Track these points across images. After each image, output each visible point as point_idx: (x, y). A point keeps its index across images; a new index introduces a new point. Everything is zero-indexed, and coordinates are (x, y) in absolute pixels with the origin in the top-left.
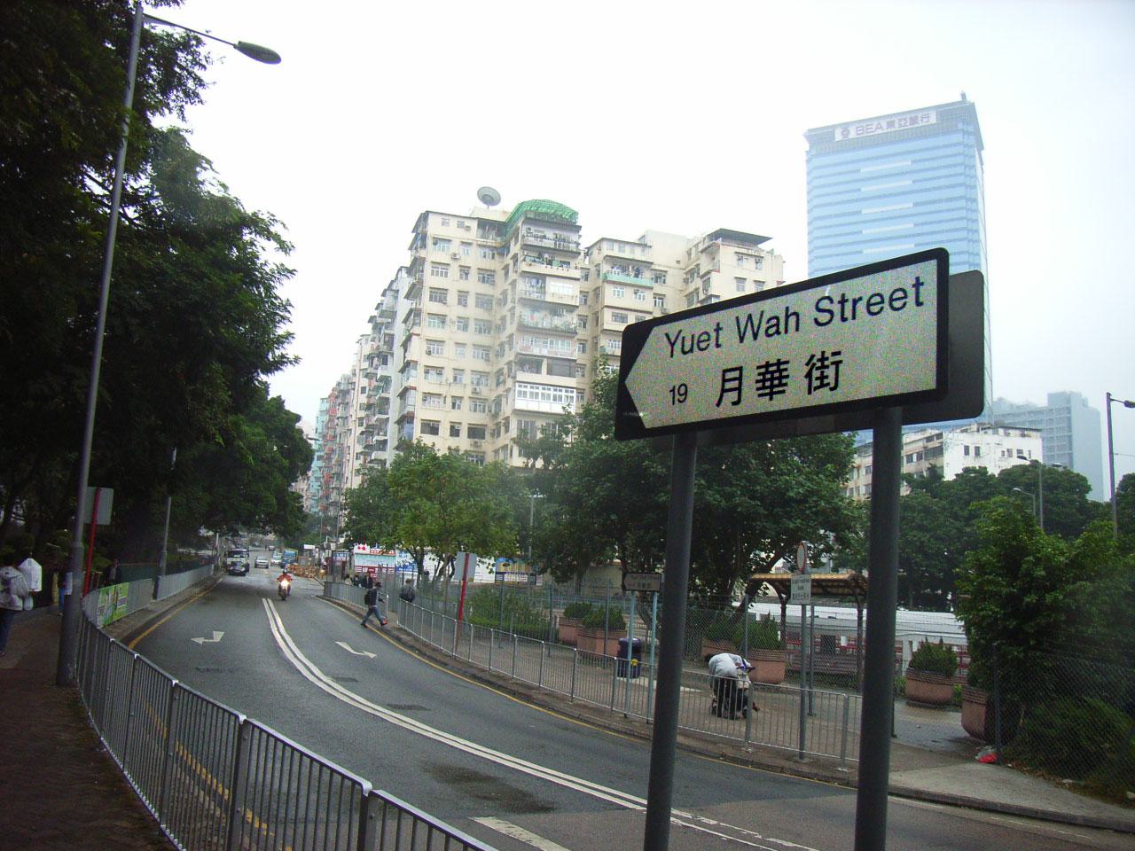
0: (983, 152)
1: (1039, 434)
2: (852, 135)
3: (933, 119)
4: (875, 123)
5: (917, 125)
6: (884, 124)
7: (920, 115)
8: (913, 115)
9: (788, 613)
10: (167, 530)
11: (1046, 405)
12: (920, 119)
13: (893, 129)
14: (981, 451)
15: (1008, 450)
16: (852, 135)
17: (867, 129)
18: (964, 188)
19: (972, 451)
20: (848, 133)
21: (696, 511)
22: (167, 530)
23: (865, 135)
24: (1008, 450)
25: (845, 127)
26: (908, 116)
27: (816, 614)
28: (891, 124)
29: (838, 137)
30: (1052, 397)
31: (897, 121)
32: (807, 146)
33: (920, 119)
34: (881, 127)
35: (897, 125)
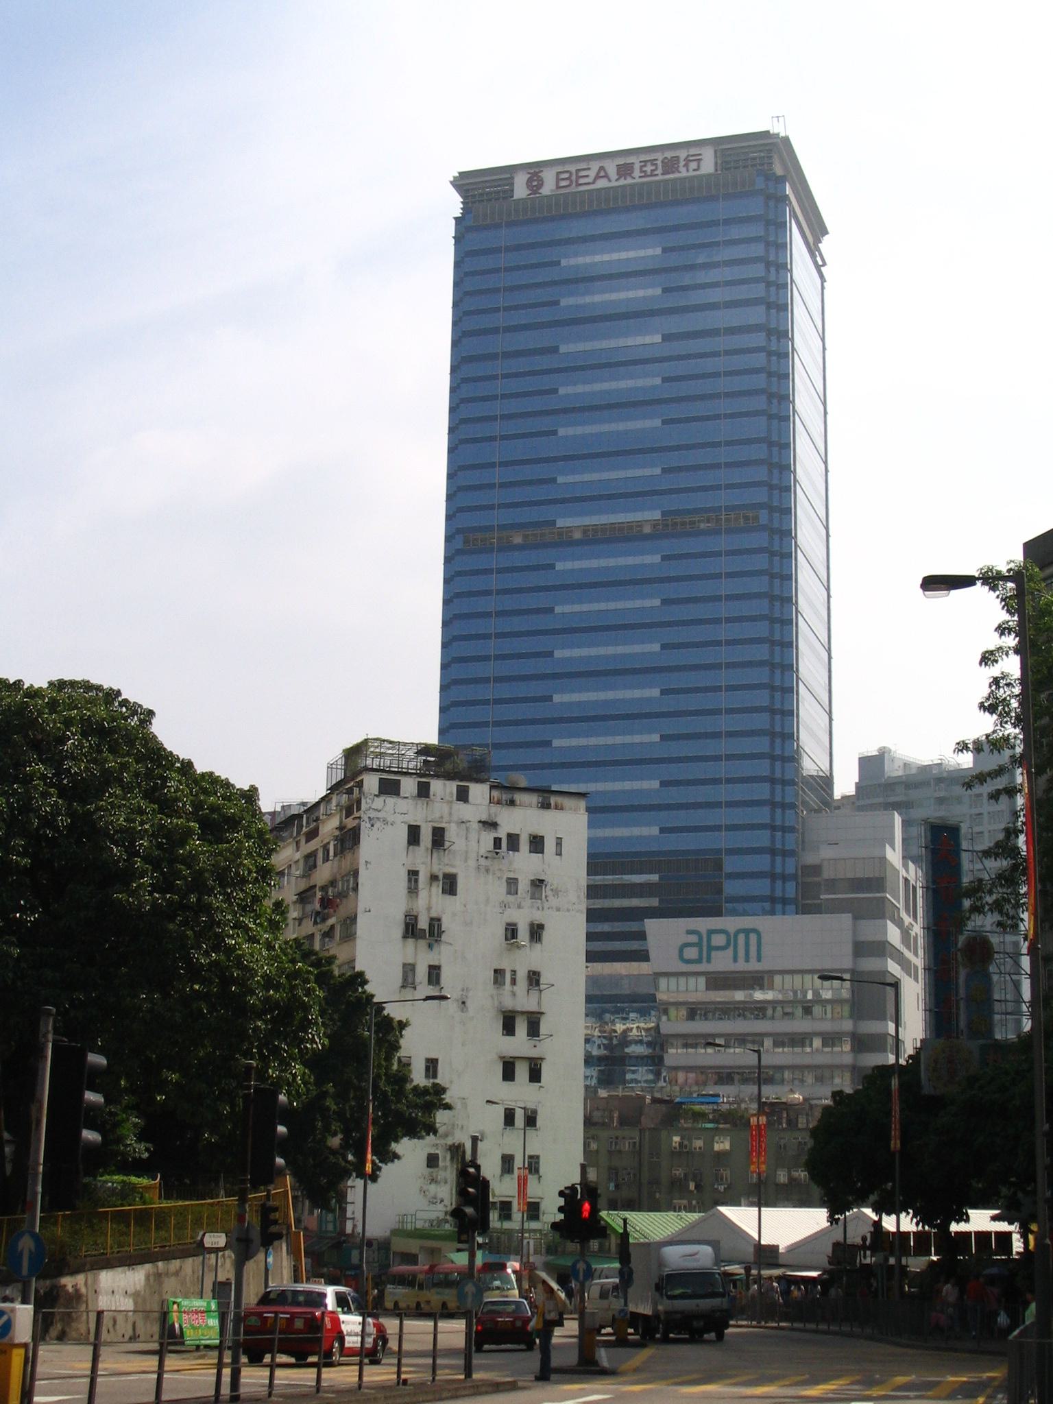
0: (826, 245)
1: (582, 804)
2: (548, 188)
3: (708, 165)
4: (595, 167)
5: (676, 175)
6: (612, 170)
7: (683, 154)
8: (669, 155)
9: (324, 1376)
10: (588, 259)
11: (971, 765)
12: (682, 163)
13: (629, 181)
14: (447, 836)
15: (510, 836)
16: (548, 188)
17: (578, 177)
18: (763, 307)
19: (426, 837)
20: (541, 185)
21: (168, 1197)
22: (588, 259)
23: (573, 189)
24: (510, 836)
25: (535, 170)
26: (659, 156)
27: (403, 1376)
28: (625, 170)
29: (521, 190)
30: (880, 749)
31: (637, 167)
32: (454, 204)
33: (682, 163)
34: (606, 176)
35: (637, 173)
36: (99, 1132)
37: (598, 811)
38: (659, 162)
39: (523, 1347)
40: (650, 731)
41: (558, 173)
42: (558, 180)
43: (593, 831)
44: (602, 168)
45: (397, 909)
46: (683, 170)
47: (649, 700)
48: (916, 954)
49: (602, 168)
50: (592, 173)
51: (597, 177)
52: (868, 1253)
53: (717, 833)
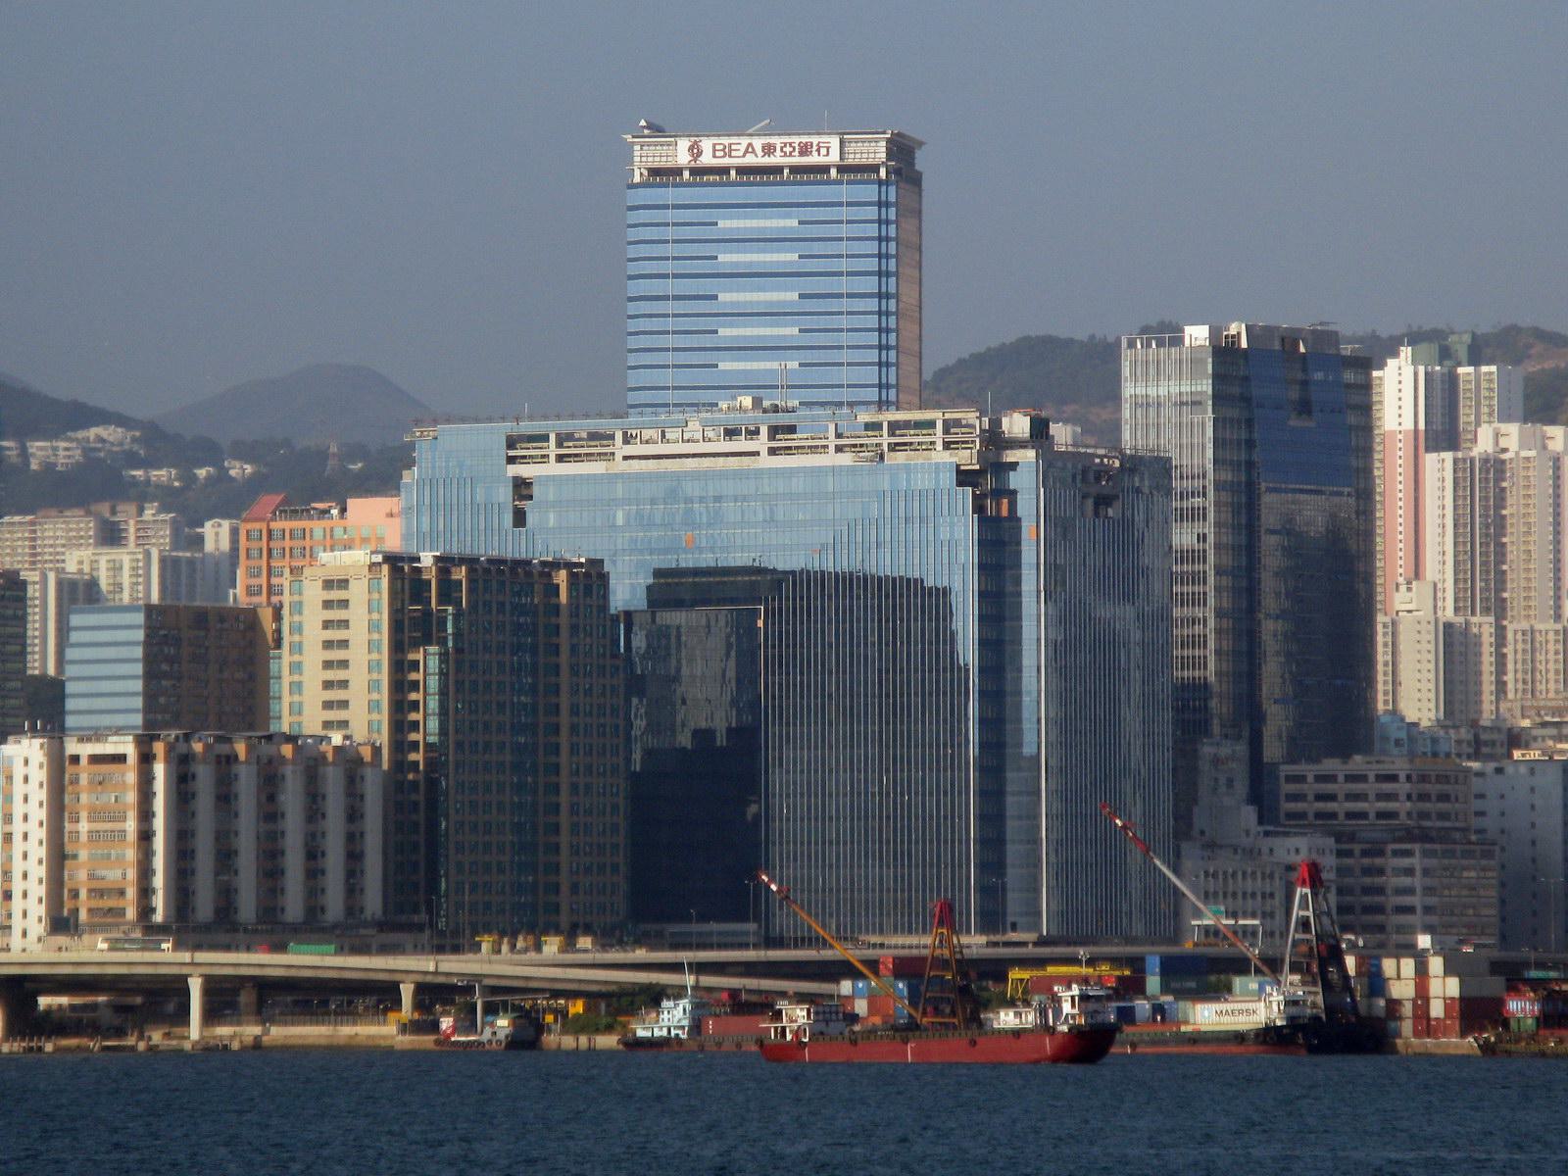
12: (815, 148)
33: (815, 148)
34: (754, 151)
36: (999, 1031)
37: (860, 932)
38: (796, 145)
39: (962, 468)
40: (792, 290)
41: (714, 145)
42: (714, 150)
43: (1426, 860)
44: (750, 145)
45: (1445, 464)
46: (815, 153)
47: (791, 262)
48: (831, 947)
49: (750, 145)
50: (743, 149)
51: (746, 152)
52: (739, 542)
53: (1401, 628)
